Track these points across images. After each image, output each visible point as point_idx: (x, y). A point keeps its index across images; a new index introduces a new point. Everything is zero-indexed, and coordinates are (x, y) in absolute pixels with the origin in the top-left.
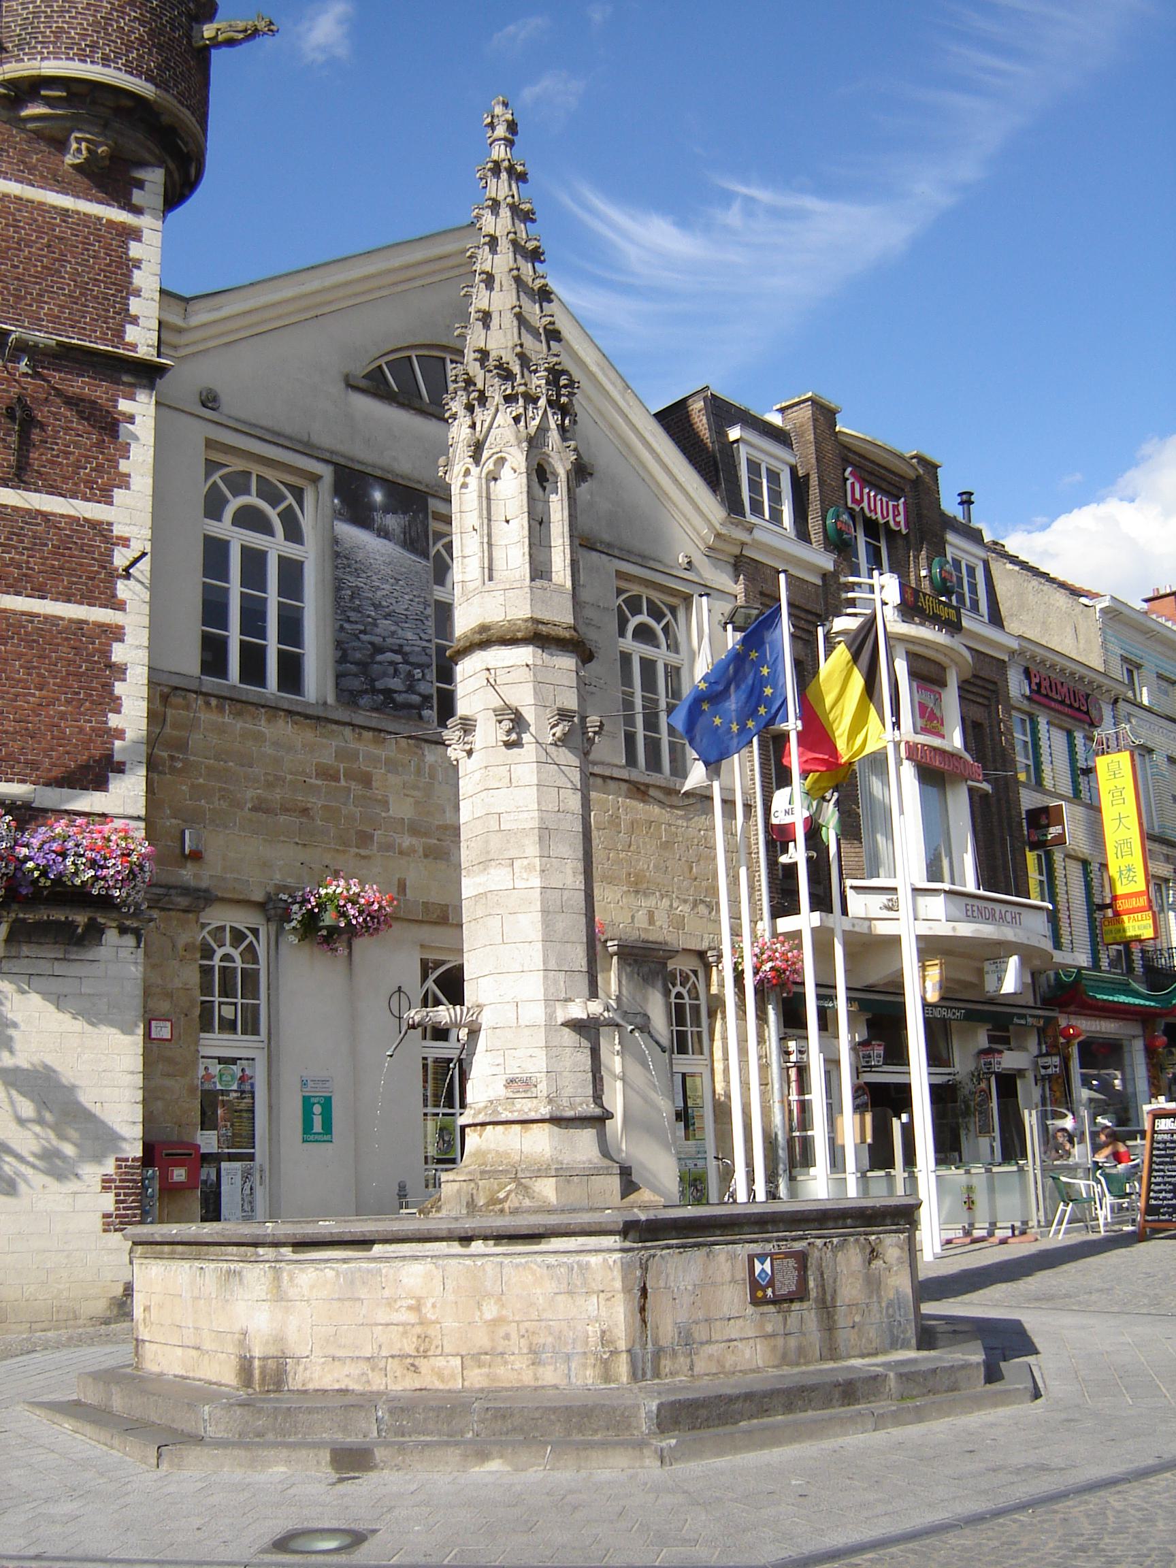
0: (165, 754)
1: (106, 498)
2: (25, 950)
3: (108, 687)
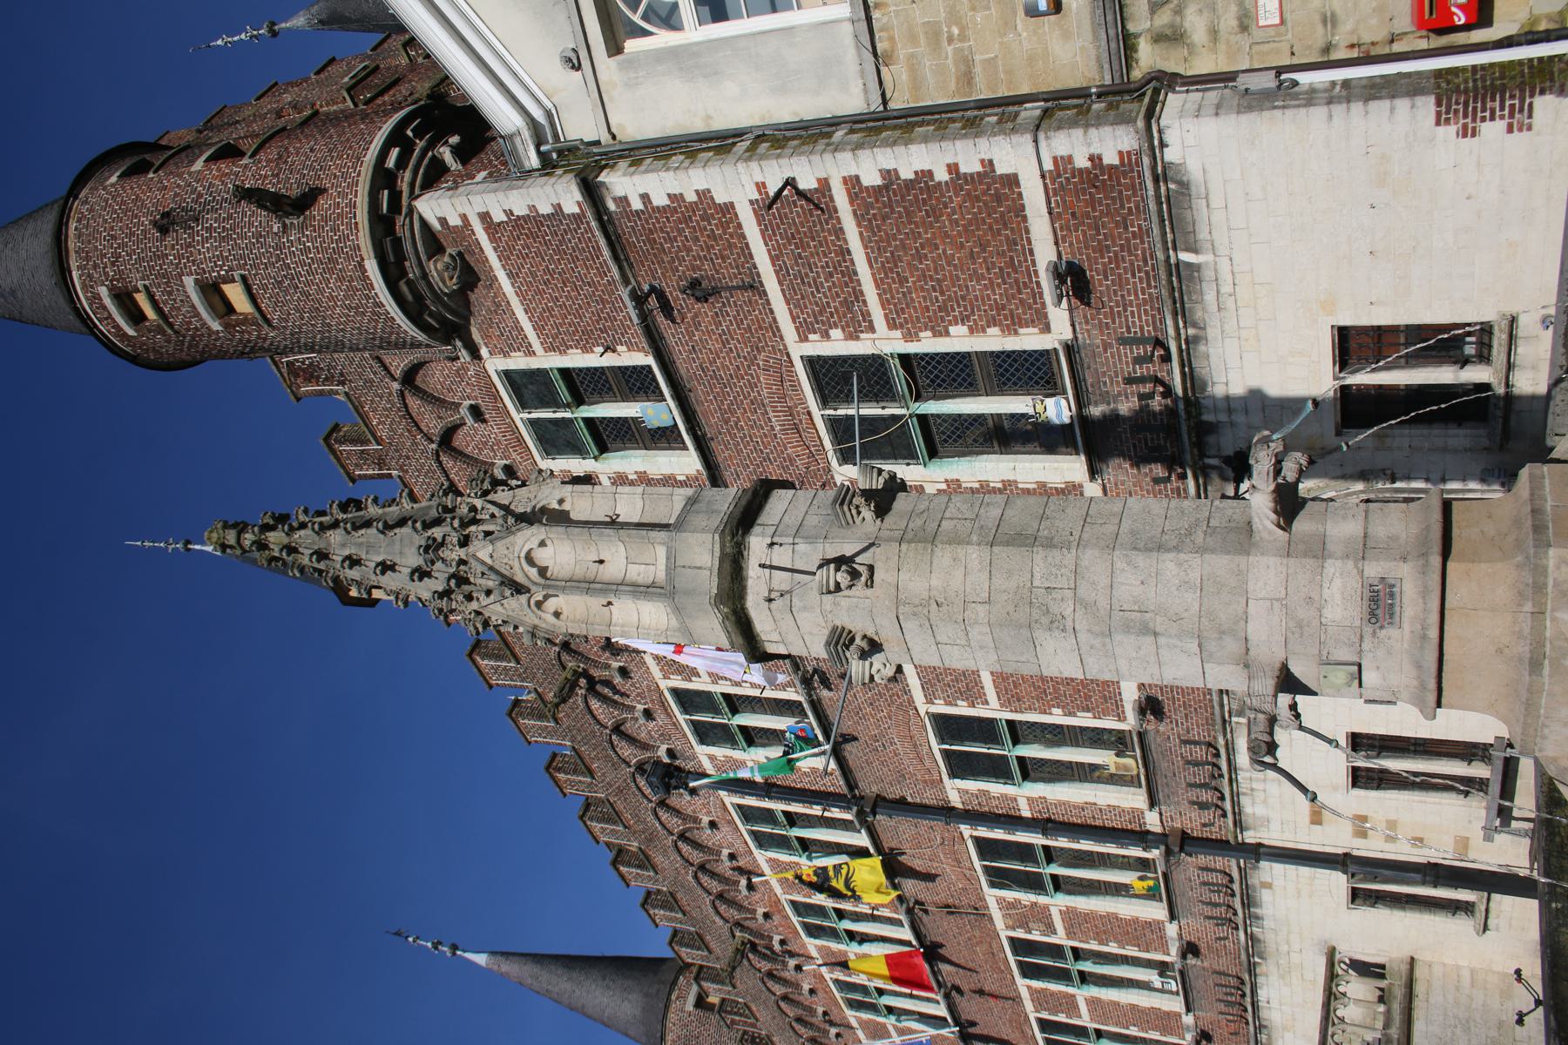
0: (950, 49)
1: (729, 208)
2: (1203, 235)
3: (909, 184)
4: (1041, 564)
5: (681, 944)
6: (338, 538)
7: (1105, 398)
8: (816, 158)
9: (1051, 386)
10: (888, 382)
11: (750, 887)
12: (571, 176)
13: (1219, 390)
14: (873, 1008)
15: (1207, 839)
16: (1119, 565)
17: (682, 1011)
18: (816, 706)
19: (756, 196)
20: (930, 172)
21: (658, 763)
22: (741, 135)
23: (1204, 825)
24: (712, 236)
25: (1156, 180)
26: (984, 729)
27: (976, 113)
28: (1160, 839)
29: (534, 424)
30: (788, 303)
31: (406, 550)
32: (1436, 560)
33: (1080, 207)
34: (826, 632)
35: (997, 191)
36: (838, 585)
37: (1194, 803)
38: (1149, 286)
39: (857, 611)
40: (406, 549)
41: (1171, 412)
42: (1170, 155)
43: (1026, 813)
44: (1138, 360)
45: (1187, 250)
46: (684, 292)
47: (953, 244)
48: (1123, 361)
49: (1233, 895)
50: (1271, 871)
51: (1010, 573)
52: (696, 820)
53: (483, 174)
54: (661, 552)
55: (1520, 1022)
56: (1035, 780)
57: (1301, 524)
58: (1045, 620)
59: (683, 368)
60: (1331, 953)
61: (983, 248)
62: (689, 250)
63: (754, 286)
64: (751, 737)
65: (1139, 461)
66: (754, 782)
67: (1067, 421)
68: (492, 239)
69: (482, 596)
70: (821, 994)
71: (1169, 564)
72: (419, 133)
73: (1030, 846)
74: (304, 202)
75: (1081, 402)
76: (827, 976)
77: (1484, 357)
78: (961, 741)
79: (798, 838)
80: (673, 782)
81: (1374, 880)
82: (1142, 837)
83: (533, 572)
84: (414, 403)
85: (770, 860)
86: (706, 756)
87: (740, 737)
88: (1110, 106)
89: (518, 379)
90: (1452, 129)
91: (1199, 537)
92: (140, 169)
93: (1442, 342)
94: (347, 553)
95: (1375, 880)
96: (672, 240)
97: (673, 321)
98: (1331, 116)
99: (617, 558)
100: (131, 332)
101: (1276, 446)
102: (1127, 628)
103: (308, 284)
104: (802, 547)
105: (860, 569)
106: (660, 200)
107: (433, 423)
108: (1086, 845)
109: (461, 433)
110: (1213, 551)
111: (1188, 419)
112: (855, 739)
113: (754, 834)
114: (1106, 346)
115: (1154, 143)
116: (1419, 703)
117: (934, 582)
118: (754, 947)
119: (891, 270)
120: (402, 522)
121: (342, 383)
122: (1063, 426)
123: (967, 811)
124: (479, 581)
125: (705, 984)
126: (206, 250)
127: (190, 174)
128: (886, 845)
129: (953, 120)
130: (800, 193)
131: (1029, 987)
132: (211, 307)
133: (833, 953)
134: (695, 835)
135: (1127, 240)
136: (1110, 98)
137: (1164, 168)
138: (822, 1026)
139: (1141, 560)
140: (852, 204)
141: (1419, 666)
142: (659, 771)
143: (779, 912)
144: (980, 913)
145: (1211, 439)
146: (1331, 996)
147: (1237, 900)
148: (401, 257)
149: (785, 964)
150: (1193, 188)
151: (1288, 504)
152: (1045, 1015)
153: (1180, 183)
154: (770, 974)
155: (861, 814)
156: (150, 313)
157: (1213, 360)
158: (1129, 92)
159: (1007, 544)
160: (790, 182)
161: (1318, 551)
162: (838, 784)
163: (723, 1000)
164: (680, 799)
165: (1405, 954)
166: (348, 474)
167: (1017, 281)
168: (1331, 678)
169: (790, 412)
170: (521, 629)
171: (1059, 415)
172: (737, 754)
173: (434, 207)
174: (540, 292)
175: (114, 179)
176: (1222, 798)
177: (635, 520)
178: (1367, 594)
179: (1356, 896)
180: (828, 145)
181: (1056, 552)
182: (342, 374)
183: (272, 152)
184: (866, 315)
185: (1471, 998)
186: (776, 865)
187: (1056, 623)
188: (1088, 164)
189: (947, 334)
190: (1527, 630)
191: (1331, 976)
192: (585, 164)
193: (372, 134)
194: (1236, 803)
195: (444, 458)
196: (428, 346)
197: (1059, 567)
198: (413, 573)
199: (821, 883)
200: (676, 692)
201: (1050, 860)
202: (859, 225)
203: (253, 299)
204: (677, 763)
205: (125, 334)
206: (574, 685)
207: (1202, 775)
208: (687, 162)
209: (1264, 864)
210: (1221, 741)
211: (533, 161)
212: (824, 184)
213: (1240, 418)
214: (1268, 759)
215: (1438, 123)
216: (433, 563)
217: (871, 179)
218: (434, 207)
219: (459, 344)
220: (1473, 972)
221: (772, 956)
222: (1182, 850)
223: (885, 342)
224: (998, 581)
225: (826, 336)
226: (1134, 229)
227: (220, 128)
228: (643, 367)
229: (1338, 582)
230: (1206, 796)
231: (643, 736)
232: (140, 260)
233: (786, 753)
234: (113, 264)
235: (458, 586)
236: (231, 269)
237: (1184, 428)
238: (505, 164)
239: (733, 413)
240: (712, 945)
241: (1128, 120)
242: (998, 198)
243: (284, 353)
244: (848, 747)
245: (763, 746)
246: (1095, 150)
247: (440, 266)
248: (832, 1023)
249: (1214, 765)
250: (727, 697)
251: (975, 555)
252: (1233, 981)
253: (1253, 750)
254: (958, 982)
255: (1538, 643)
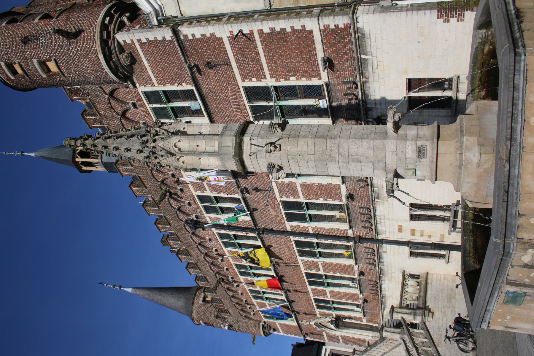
1: (220, 39)
2: (368, 50)
3: (279, 32)
4: (329, 144)
5: (199, 280)
6: (111, 142)
7: (338, 100)
8: (249, 24)
9: (320, 96)
10: (270, 95)
11: (222, 260)
12: (168, 28)
13: (372, 98)
14: (261, 298)
15: (367, 238)
16: (351, 143)
17: (198, 303)
18: (245, 199)
19: (229, 35)
20: (285, 29)
21: (192, 220)
22: (224, 16)
23: (366, 233)
24: (215, 48)
25: (355, 33)
26: (298, 205)
27: (299, 10)
28: (353, 239)
29: (153, 109)
30: (239, 70)
31: (134, 144)
32: (436, 140)
33: (332, 40)
34: (267, 165)
35: (306, 36)
36: (271, 150)
37: (363, 227)
38: (352, 65)
39: (276, 158)
40: (135, 144)
41: (358, 104)
42: (359, 25)
43: (311, 232)
44: (348, 88)
45: (364, 54)
46: (205, 66)
47: (292, 51)
48: (344, 88)
49: (375, 256)
50: (386, 247)
51: (320, 146)
52: (205, 239)
53: (138, 26)
54: (217, 143)
55: (457, 287)
56: (314, 221)
57: (400, 131)
58: (330, 159)
59: (204, 90)
60: (404, 272)
61: (301, 52)
62: (207, 52)
63: (228, 64)
64: (223, 210)
65: (348, 119)
66: (224, 225)
67: (326, 107)
68: (142, 48)
69: (160, 157)
70: (244, 294)
71: (364, 143)
72: (116, 12)
73: (312, 243)
74: (77, 34)
75: (330, 102)
76: (247, 288)
77: (450, 88)
78: (291, 210)
79: (238, 243)
80: (198, 226)
81: (417, 249)
82: (347, 238)
83: (177, 150)
84: (113, 102)
85: (229, 251)
86: (208, 217)
87: (219, 211)
88: (341, 10)
89: (149, 94)
90: (442, 20)
91: (373, 135)
92: (13, 21)
93: (438, 84)
94: (114, 146)
95: (417, 248)
96: (202, 49)
97: (201, 75)
98: (407, 15)
99: (203, 145)
100: (12, 78)
101: (394, 110)
102: (353, 161)
103: (78, 62)
104: (260, 140)
105: (278, 146)
106: (198, 36)
107: (120, 109)
108: (330, 242)
109: (128, 112)
110: (377, 139)
111: (363, 106)
112: (257, 210)
113: (223, 242)
114: (338, 84)
115: (354, 21)
116: (431, 179)
117: (299, 149)
118: (223, 279)
119: (272, 59)
120: (132, 136)
121: (88, 96)
122: (325, 109)
123: (292, 232)
124: (159, 153)
125: (207, 293)
126: (41, 50)
127: (34, 24)
128: (266, 244)
129: (292, 13)
130: (244, 35)
131: (311, 288)
132: (43, 70)
133: (249, 281)
134: (204, 244)
135: (346, 51)
136: (341, 7)
137: (357, 29)
138: (245, 305)
139: (357, 141)
140: (260, 38)
141: (431, 169)
142: (193, 223)
143: (231, 268)
144: (296, 265)
145: (370, 113)
146: (404, 285)
147: (376, 257)
148: (111, 53)
149: (233, 285)
150: (366, 36)
151: (397, 127)
152: (316, 297)
153: (362, 34)
154: (228, 289)
155: (259, 234)
156: (20, 71)
157: (371, 88)
158: (347, 5)
159: (319, 138)
160: (241, 31)
161: (405, 138)
162: (252, 225)
163: (212, 299)
164: (200, 232)
165: (425, 271)
166: (89, 126)
167: (311, 63)
168: (408, 173)
169: (239, 104)
170: (171, 167)
171: (323, 105)
172: (218, 216)
173: (122, 37)
174: (157, 65)
175: (4, 24)
176: (372, 225)
177: (208, 133)
178: (418, 150)
179: (412, 254)
180: (253, 19)
181: (333, 140)
182: (88, 93)
183: (64, 17)
184: (264, 74)
185: (444, 283)
186: (230, 252)
187: (333, 160)
188: (334, 27)
189: (289, 80)
190: (458, 158)
191: (404, 279)
192: (174, 24)
193: (100, 12)
194: (376, 227)
195: (123, 121)
196: (119, 83)
197: (334, 144)
198: (138, 151)
199: (246, 257)
200: (199, 196)
201: (318, 247)
202: (262, 45)
203: (58, 67)
204: (199, 220)
205: (10, 79)
206: (165, 195)
207: (366, 217)
208: (207, 24)
209: (384, 245)
210: (372, 207)
211: (155, 22)
212: (252, 32)
213: (379, 106)
214: (392, 194)
215: (438, 18)
216: (144, 148)
217: (267, 30)
218: (122, 37)
219: (129, 82)
220: (444, 275)
221: (229, 283)
222: (359, 242)
223: (269, 82)
224: (317, 148)
225: (251, 80)
226: (347, 47)
227: (35, 7)
228: (190, 90)
229: (410, 147)
230: (367, 224)
231: (187, 211)
232: (16, 53)
233: (235, 215)
234: (6, 54)
235: (153, 154)
236: (50, 57)
237: (362, 109)
238: (146, 23)
239: (220, 105)
240: (209, 280)
241: (347, 14)
242: (306, 37)
243: (68, 85)
244: (255, 212)
245: (227, 213)
246: (337, 23)
247: (124, 57)
248: (248, 304)
249: (370, 215)
250: (215, 197)
251: (310, 141)
252: (374, 283)
253: (388, 192)
254: (289, 288)
255: (461, 161)
